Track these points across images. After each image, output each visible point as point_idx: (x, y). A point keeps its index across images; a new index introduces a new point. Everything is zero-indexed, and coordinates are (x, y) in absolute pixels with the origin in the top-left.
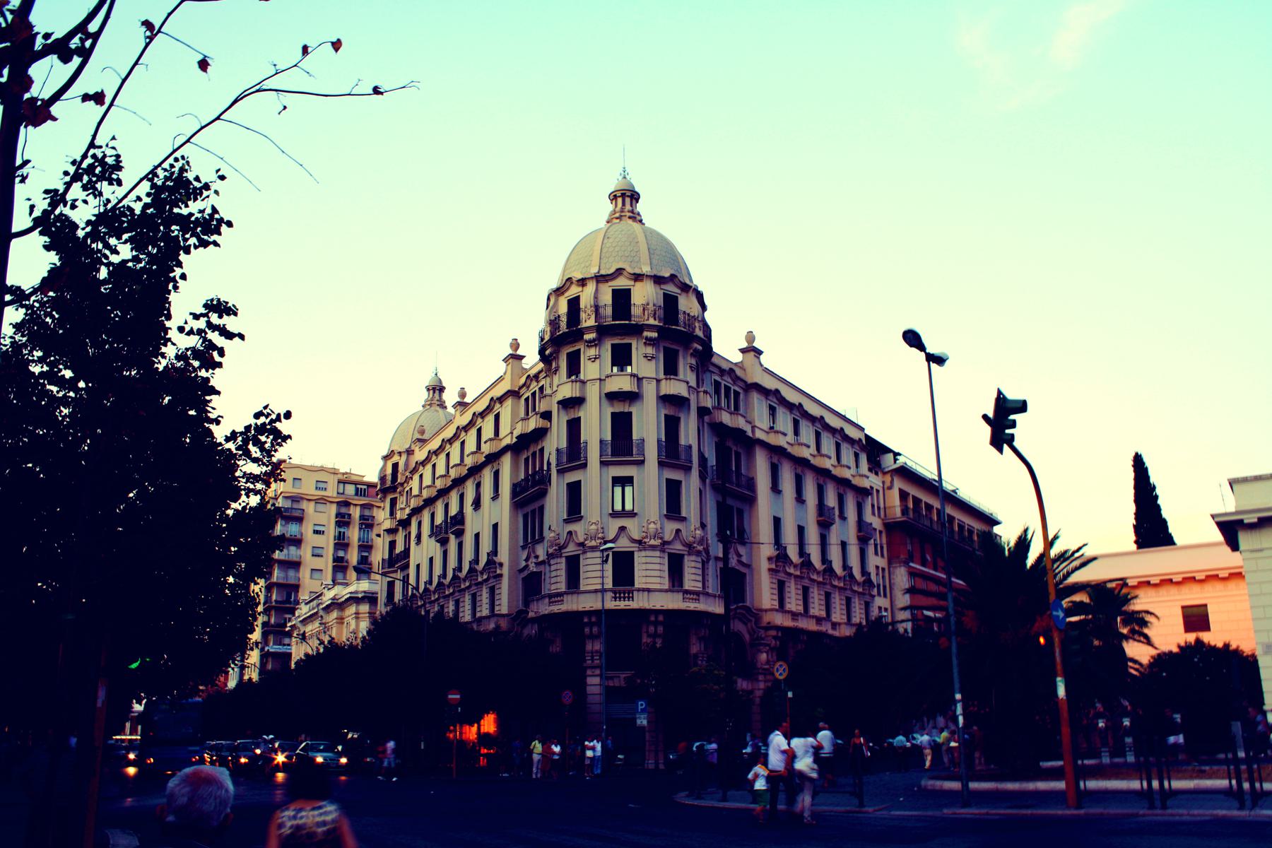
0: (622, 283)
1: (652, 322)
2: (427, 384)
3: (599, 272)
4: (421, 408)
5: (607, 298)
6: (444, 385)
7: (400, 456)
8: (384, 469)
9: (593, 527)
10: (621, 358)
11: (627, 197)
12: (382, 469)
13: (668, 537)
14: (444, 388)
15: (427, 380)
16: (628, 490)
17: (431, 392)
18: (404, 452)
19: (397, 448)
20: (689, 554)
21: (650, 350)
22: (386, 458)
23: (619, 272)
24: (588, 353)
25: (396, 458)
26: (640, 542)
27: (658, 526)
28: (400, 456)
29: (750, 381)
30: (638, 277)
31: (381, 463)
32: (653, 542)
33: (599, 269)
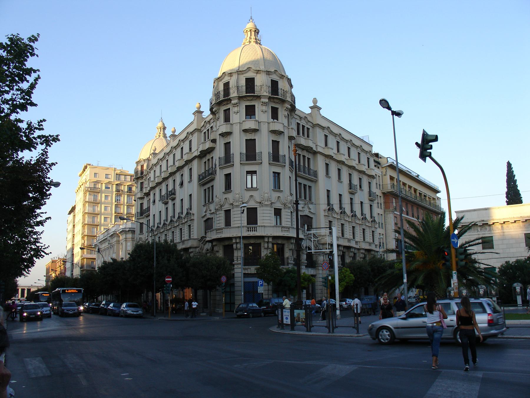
5: (243, 83)
16: (254, 177)
21: (264, 108)
30: (258, 72)
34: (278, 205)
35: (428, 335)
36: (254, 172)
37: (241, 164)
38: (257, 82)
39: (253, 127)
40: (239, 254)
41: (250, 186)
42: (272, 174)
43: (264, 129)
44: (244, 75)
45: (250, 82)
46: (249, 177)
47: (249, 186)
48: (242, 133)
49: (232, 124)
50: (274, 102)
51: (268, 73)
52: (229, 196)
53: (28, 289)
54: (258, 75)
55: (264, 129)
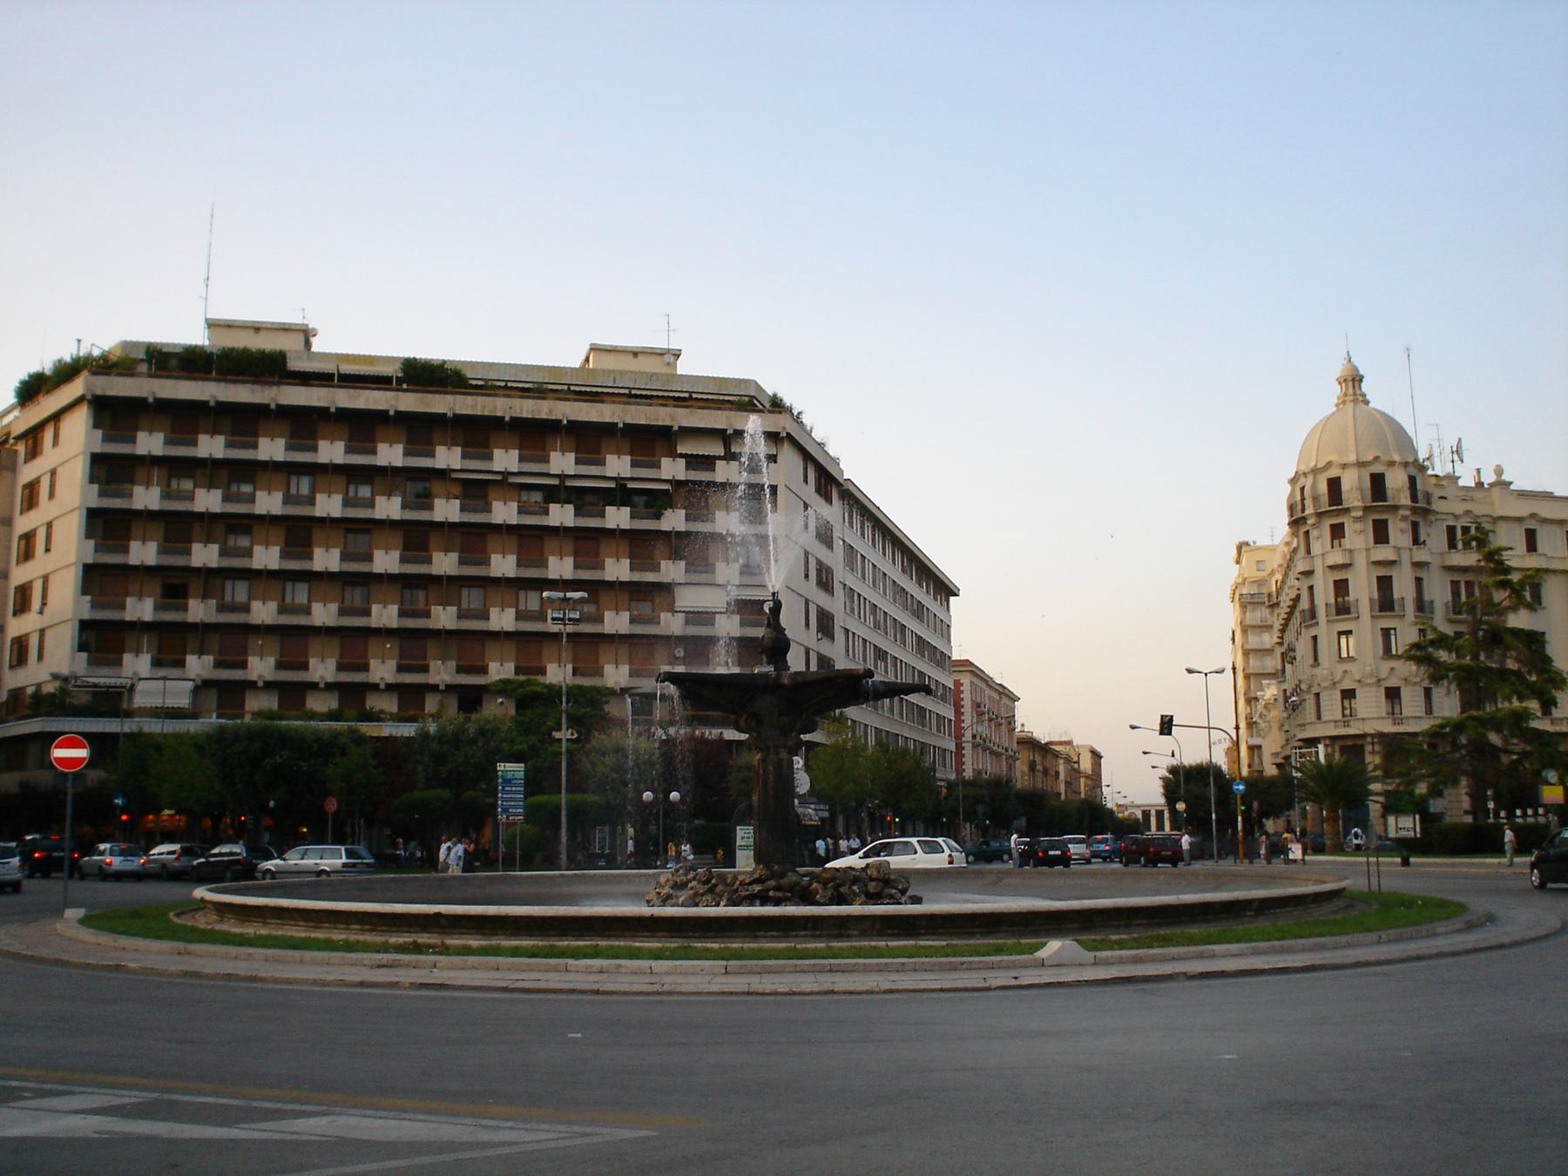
0: (1333, 473)
1: (1356, 504)
2: (1338, 375)
3: (1316, 465)
4: (1335, 409)
5: (1323, 488)
6: (1362, 373)
7: (1306, 477)
8: (1291, 495)
9: (1325, 672)
10: (1337, 532)
11: (1353, 380)
12: (1290, 495)
13: (1383, 675)
14: (1363, 377)
15: (1337, 369)
16: (1351, 640)
17: (1344, 385)
18: (1309, 472)
19: (1303, 468)
20: (1406, 686)
21: (1358, 526)
22: (1293, 481)
23: (1329, 464)
24: (1314, 533)
25: (1302, 481)
26: (1359, 681)
27: (1374, 667)
28: (1306, 477)
29: (1495, 515)
30: (1344, 466)
31: (1289, 488)
32: (1369, 681)
33: (1317, 462)
34: (1393, 683)
35: (374, 859)
36: (1348, 633)
37: (1372, 616)
38: (1346, 486)
39: (1340, 561)
40: (1373, 759)
41: (1346, 656)
42: (1380, 633)
43: (1361, 562)
44: (1324, 474)
45: (1334, 484)
46: (1343, 640)
47: (1344, 655)
48: (1327, 571)
49: (1313, 557)
50: (1379, 512)
51: (1361, 464)
52: (1316, 671)
53: (1157, 811)
54: (1346, 471)
55: (1361, 562)
